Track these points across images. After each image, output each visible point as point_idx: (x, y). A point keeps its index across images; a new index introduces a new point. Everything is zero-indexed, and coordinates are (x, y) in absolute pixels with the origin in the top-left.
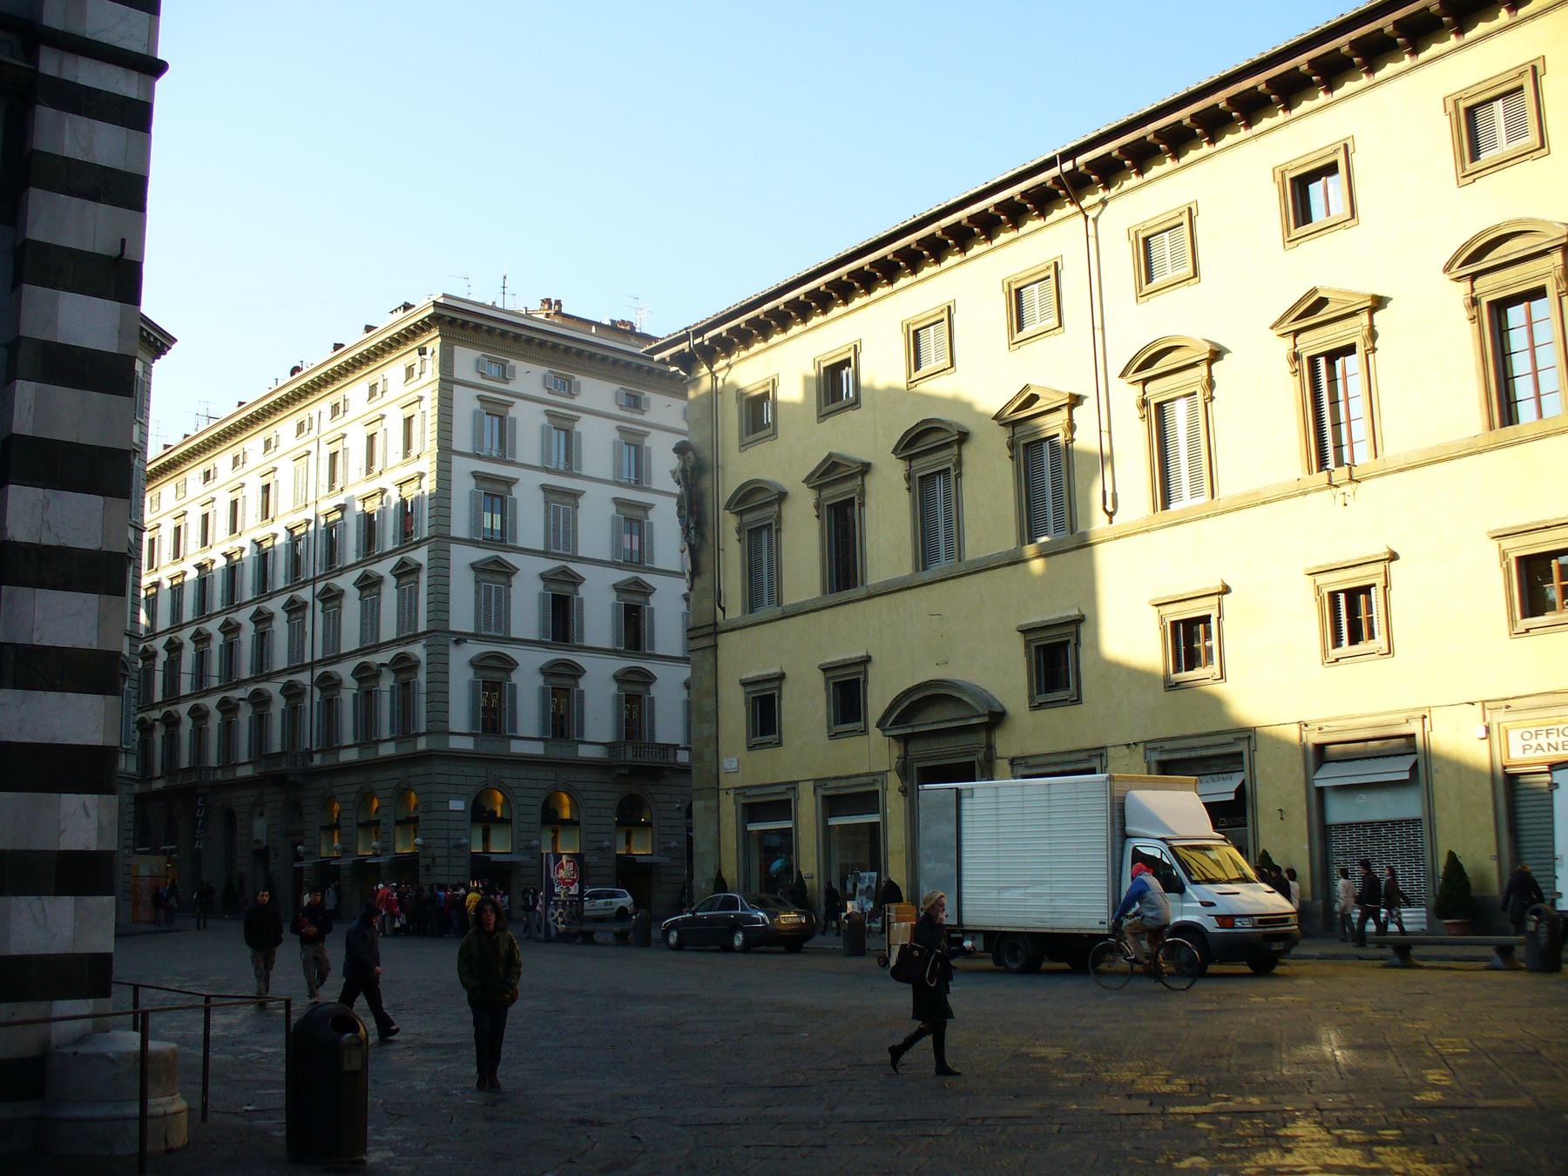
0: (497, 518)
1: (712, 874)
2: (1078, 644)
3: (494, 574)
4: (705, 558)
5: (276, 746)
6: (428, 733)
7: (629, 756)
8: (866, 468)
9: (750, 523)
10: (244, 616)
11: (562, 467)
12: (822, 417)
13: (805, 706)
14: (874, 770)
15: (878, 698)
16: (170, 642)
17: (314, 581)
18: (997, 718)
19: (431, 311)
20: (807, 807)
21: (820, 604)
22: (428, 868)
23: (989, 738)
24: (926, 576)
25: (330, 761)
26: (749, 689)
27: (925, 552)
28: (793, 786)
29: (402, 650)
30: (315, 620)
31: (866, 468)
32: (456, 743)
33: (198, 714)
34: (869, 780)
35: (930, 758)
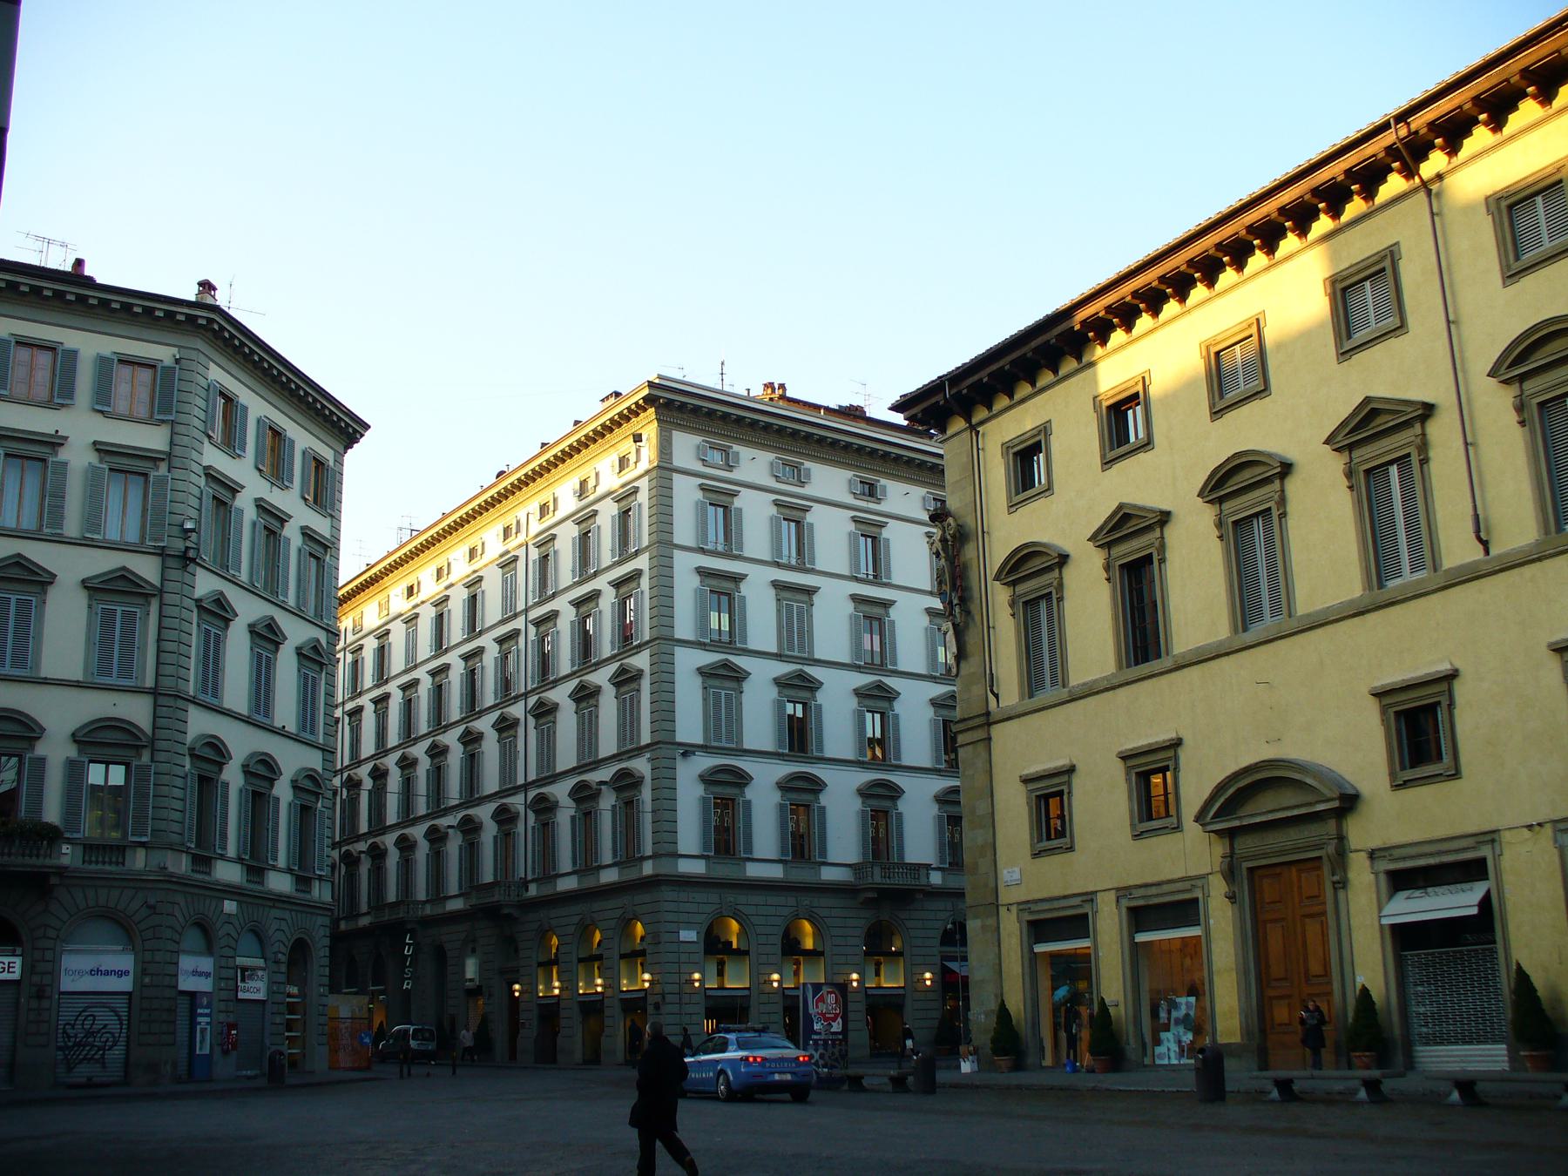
0: (725, 618)
1: (993, 1005)
2: (1451, 705)
3: (724, 679)
4: (972, 639)
5: (488, 876)
6: (655, 856)
7: (877, 878)
8: (1164, 518)
9: (1025, 594)
10: (451, 739)
11: (793, 562)
12: (1107, 463)
13: (1102, 802)
14: (1192, 873)
15: (1196, 784)
16: (375, 768)
17: (526, 695)
18: (1349, 802)
19: (646, 392)
20: (1109, 924)
21: (1116, 682)
22: (657, 1006)
23: (1339, 827)
24: (1248, 637)
25: (547, 890)
26: (1032, 786)
27: (1245, 608)
28: (1090, 897)
29: (624, 765)
30: (528, 738)
31: (1164, 518)
32: (686, 867)
33: (406, 845)
34: (1187, 885)
35: (1265, 855)
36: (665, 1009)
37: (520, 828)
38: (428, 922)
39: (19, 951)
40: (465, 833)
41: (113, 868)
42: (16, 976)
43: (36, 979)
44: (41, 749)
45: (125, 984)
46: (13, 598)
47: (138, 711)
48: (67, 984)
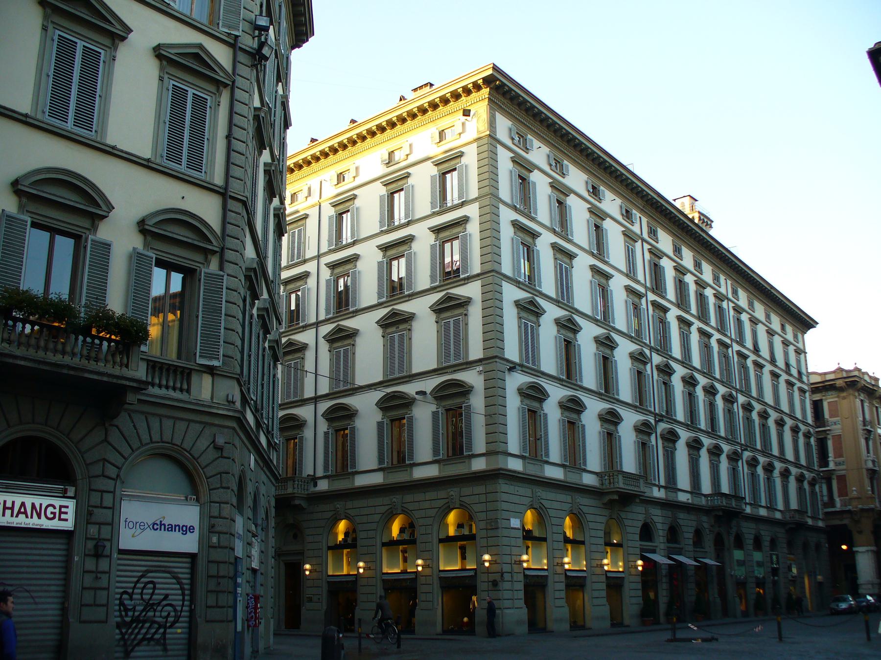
17: (317, 324)
19: (490, 72)
22: (495, 583)
37: (308, 433)
39: (71, 491)
41: (177, 395)
42: (68, 525)
43: (93, 530)
44: (104, 232)
45: (189, 544)
46: (80, 44)
47: (206, 208)
48: (128, 540)
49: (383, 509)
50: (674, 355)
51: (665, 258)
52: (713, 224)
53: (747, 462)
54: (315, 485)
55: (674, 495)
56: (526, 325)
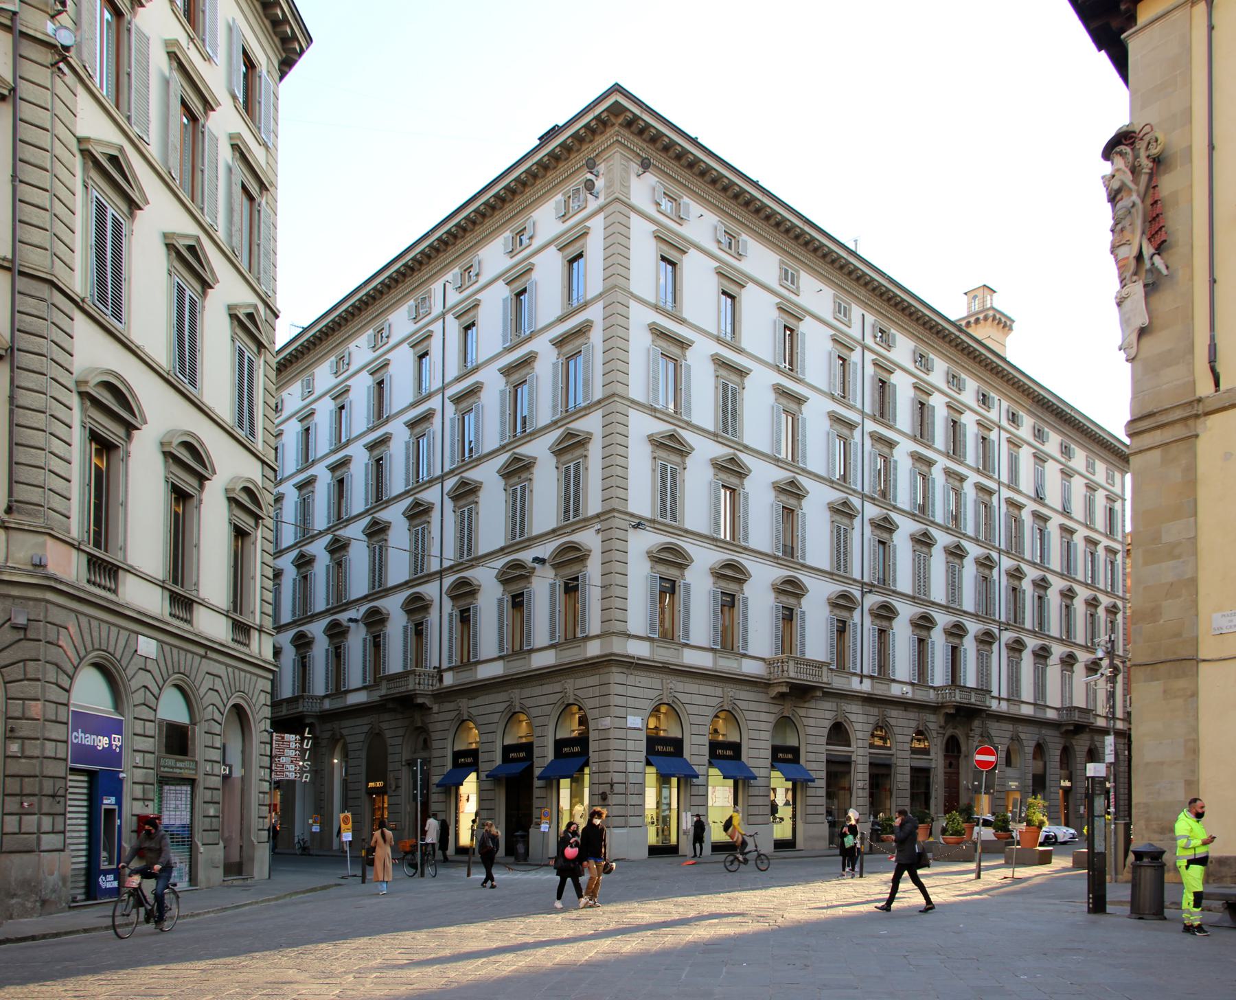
6: (602, 635)
17: (442, 478)
25: (465, 677)
36: (612, 799)
38: (328, 717)
40: (368, 625)
49: (502, 707)
50: (899, 505)
51: (898, 372)
52: (1014, 326)
53: (1007, 645)
54: (441, 680)
55: (884, 687)
56: (664, 468)
